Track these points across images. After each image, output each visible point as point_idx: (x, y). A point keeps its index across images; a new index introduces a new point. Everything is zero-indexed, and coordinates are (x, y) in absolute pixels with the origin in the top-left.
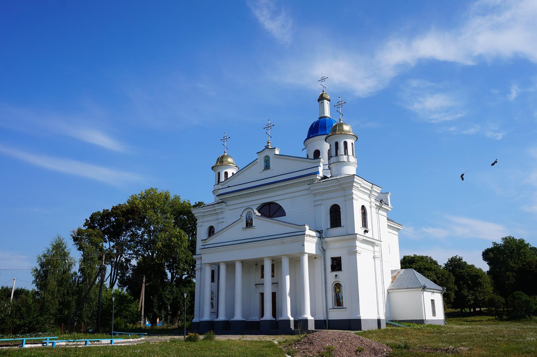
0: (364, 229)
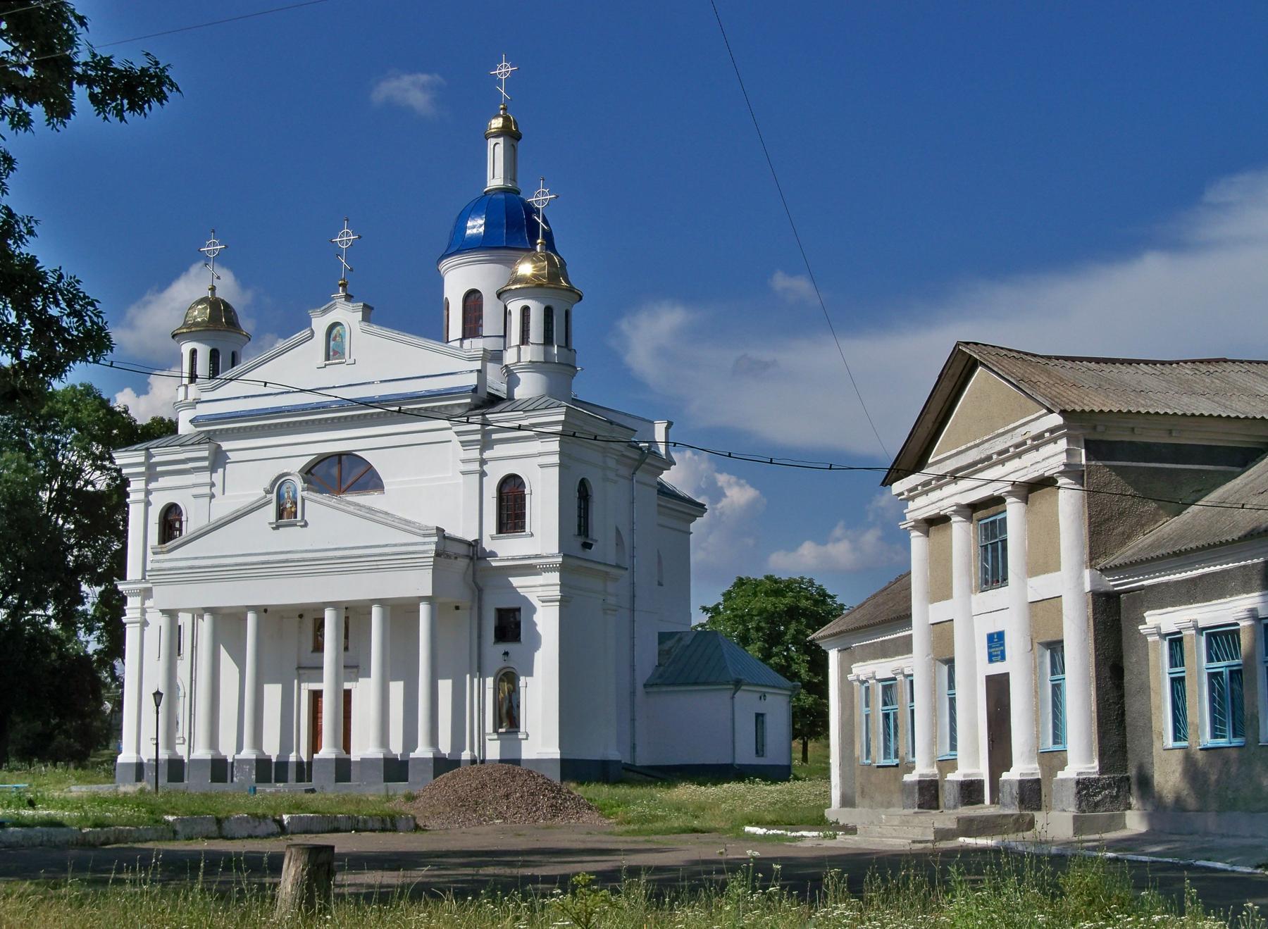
0: (581, 540)
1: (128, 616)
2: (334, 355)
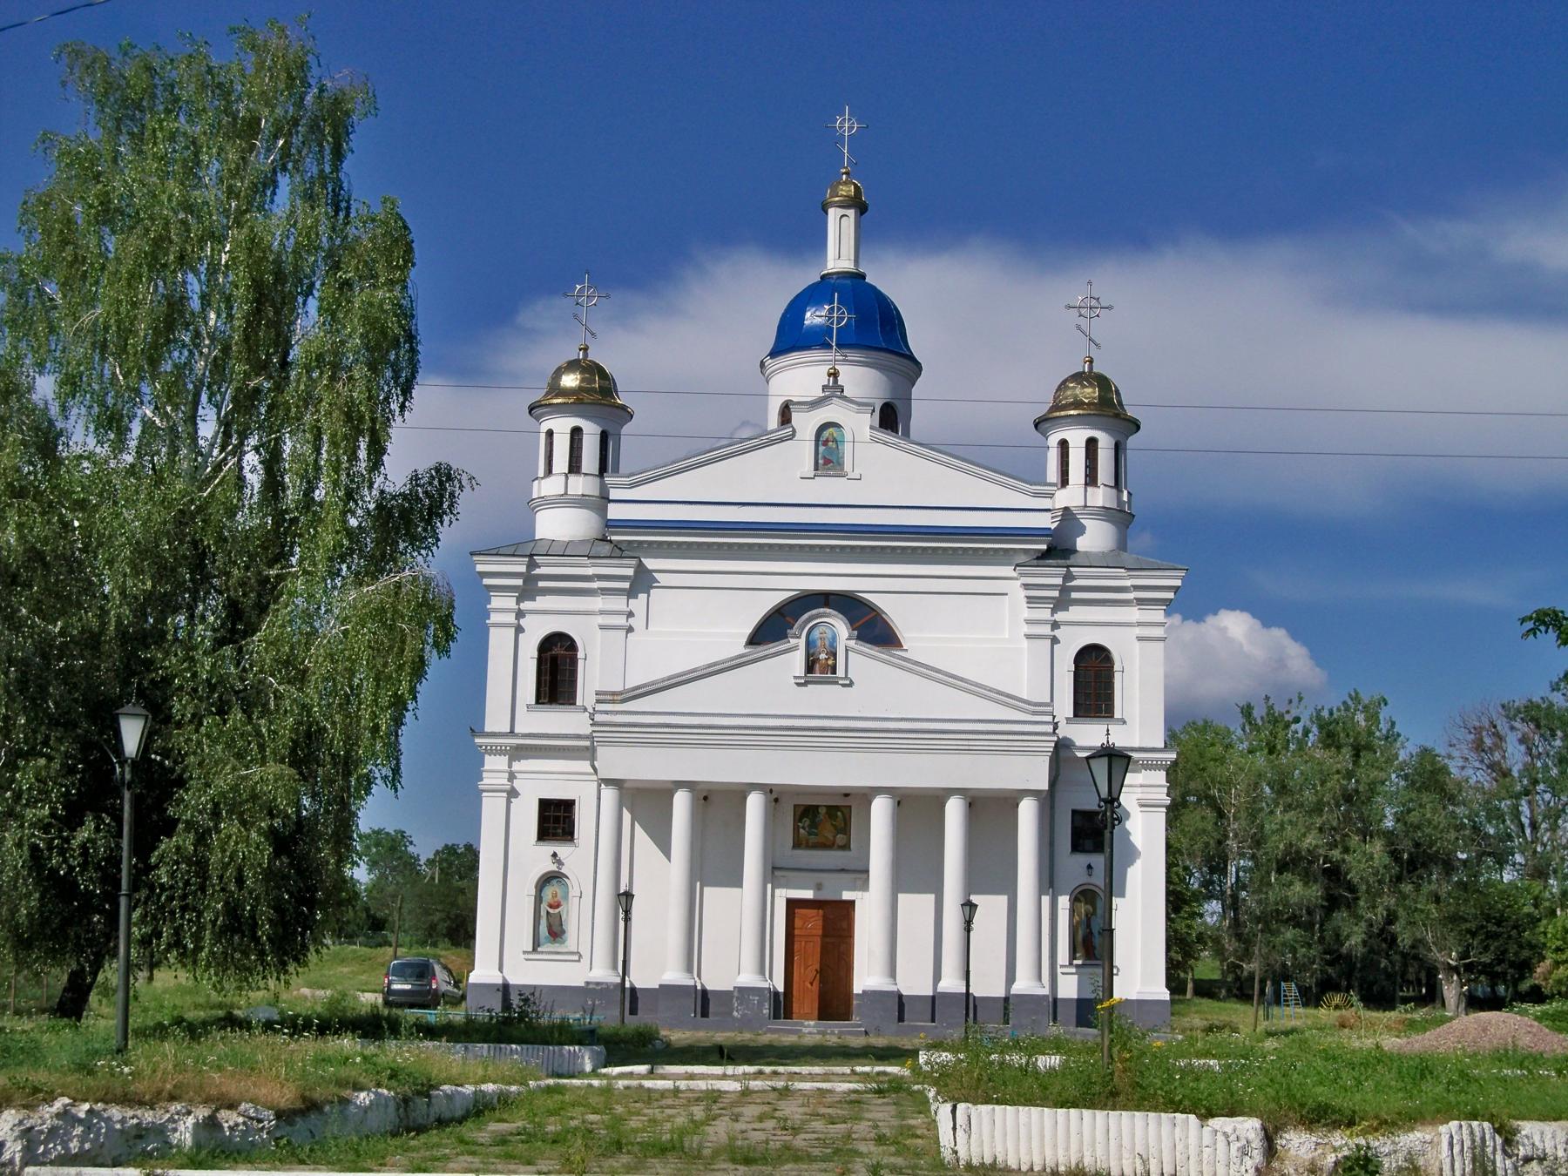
1: (485, 781)
2: (825, 464)
